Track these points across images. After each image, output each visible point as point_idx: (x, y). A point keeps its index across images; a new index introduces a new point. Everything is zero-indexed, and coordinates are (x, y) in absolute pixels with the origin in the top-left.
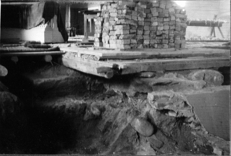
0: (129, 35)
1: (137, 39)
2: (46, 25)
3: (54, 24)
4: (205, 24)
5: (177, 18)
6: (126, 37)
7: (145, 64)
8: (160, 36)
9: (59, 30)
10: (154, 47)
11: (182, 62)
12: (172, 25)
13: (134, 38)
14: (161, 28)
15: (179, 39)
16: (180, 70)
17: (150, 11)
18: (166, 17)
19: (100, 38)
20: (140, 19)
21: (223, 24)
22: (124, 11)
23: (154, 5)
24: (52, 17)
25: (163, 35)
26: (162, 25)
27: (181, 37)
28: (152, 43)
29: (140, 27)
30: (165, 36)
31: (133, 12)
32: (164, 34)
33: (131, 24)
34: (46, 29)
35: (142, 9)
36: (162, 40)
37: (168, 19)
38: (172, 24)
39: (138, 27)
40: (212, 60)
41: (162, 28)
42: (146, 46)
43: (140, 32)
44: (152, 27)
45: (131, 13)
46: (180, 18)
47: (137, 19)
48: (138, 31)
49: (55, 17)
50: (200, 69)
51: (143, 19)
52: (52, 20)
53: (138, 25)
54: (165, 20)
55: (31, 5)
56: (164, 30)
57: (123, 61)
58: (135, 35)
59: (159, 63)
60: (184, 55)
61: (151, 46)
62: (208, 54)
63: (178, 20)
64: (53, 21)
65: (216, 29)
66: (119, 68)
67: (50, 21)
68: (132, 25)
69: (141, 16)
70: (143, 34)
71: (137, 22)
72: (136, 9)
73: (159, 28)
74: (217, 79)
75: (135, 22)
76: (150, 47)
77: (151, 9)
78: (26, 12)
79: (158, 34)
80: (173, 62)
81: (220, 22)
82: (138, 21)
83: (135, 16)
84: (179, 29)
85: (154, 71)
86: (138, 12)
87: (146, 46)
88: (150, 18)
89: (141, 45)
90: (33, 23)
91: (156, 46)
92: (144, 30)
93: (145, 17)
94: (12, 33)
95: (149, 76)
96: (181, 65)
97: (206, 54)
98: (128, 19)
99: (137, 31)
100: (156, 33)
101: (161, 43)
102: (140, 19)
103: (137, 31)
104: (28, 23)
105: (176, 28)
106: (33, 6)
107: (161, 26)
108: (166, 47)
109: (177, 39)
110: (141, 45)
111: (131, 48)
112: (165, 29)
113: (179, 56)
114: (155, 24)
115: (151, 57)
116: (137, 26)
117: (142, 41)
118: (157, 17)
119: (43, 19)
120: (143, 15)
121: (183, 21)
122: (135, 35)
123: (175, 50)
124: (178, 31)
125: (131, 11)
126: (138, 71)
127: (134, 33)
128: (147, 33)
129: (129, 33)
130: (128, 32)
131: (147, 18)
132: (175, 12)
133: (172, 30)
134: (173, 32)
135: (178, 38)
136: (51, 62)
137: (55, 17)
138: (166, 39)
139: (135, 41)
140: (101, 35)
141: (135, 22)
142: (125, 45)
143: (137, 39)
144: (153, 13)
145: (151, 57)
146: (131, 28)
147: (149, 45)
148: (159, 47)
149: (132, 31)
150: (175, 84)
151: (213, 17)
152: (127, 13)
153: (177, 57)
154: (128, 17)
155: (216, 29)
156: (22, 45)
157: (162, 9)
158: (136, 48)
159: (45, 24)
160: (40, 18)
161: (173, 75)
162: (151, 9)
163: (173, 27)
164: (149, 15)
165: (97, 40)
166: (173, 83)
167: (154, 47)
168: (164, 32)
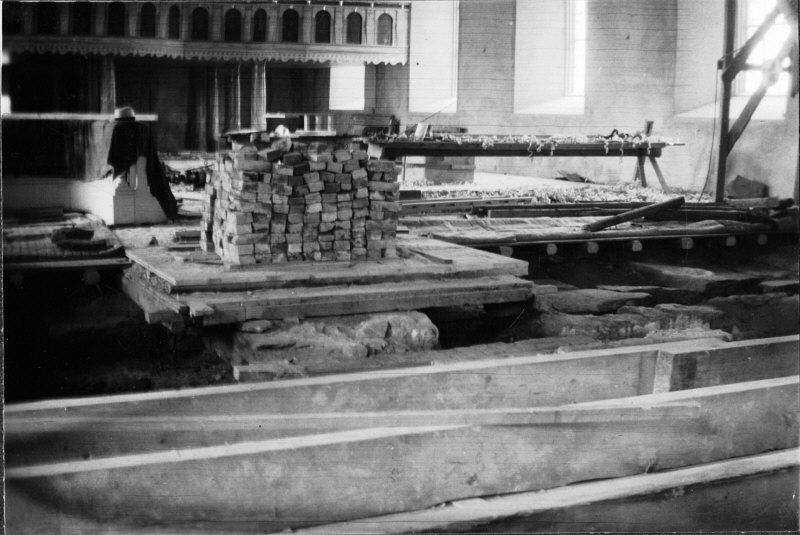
0: (250, 236)
1: (270, 243)
2: (118, 180)
3: (138, 176)
4: (604, 150)
5: (374, 192)
6: (244, 239)
7: (258, 304)
8: (331, 232)
9: (154, 192)
10: (312, 259)
11: (352, 296)
12: (361, 209)
13: (263, 241)
14: (330, 217)
15: (379, 238)
16: (342, 315)
17: (303, 179)
18: (343, 192)
19: (209, 233)
20: (277, 199)
21: (664, 151)
22: (240, 184)
23: (313, 166)
24: (134, 161)
25: (337, 232)
26: (335, 209)
27: (383, 234)
28: (307, 249)
29: (276, 216)
30: (342, 232)
31: (260, 184)
32: (340, 228)
33: (256, 211)
34: (119, 191)
35: (282, 178)
36: (333, 242)
37: (348, 195)
38: (361, 205)
39: (273, 218)
40: (433, 291)
41: (333, 217)
42: (290, 258)
43: (279, 227)
44: (308, 216)
45: (255, 187)
46: (383, 193)
47: (271, 199)
48: (274, 225)
49: (142, 162)
50: (396, 310)
51: (286, 200)
52: (132, 169)
53: (273, 212)
54: (341, 198)
55: (93, 121)
56: (338, 220)
57: (224, 294)
58: (266, 234)
59: (290, 301)
60: (374, 277)
61: (303, 257)
62: (443, 272)
63: (376, 195)
64: (136, 172)
65: (648, 165)
66: (177, 312)
67: (128, 171)
68: (259, 214)
69: (281, 191)
70: (287, 231)
71: (271, 207)
72: (267, 178)
73: (325, 217)
74: (419, 336)
75: (264, 206)
76: (304, 259)
77: (306, 176)
78: (80, 138)
79: (323, 228)
80: (327, 298)
81: (652, 144)
82: (273, 204)
83: (264, 192)
84: (380, 216)
85: (275, 319)
86: (272, 186)
87: (295, 257)
88: (304, 196)
89: (282, 256)
90: (96, 169)
91: (318, 256)
92: (288, 223)
93: (290, 193)
94: (42, 191)
95: (258, 329)
96: (344, 304)
97: (436, 273)
98: (247, 201)
99: (270, 226)
100: (318, 228)
101: (330, 251)
102: (277, 199)
103: (270, 226)
104: (87, 167)
105: (372, 214)
106: (95, 124)
107: (330, 212)
108: (344, 258)
109: (373, 238)
110: (282, 256)
111: (258, 262)
112: (342, 217)
113: (363, 280)
114: (315, 208)
115: (291, 285)
116: (269, 216)
117: (283, 247)
118: (321, 192)
119: (110, 167)
120: (284, 191)
121: (389, 197)
122: (266, 234)
123: (350, 266)
124: (376, 220)
125: (254, 183)
126: (241, 317)
127: (262, 231)
128: (296, 227)
129: (250, 231)
130: (248, 229)
131: (294, 195)
132: (366, 179)
133: (360, 219)
134: (363, 224)
135: (375, 238)
136: (98, 286)
137: (142, 162)
138: (342, 238)
139: (265, 247)
140: (210, 226)
141: (264, 206)
142: (241, 256)
143: (270, 243)
144: (310, 185)
145: (291, 285)
146: (255, 221)
147: (302, 253)
148: (325, 258)
149: (257, 226)
150: (302, 347)
151: (642, 128)
152: (246, 188)
153: (357, 282)
154: (247, 196)
155: (648, 165)
156: (213, 13)
157: (335, 173)
158: (268, 261)
159: (115, 177)
160: (106, 167)
161: (538, 321)
162: (306, 176)
163: (364, 213)
164: (301, 190)
165: (203, 236)
166: (298, 345)
167: (312, 259)
168: (338, 224)
